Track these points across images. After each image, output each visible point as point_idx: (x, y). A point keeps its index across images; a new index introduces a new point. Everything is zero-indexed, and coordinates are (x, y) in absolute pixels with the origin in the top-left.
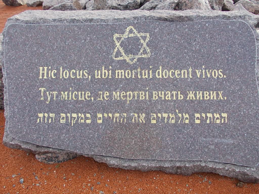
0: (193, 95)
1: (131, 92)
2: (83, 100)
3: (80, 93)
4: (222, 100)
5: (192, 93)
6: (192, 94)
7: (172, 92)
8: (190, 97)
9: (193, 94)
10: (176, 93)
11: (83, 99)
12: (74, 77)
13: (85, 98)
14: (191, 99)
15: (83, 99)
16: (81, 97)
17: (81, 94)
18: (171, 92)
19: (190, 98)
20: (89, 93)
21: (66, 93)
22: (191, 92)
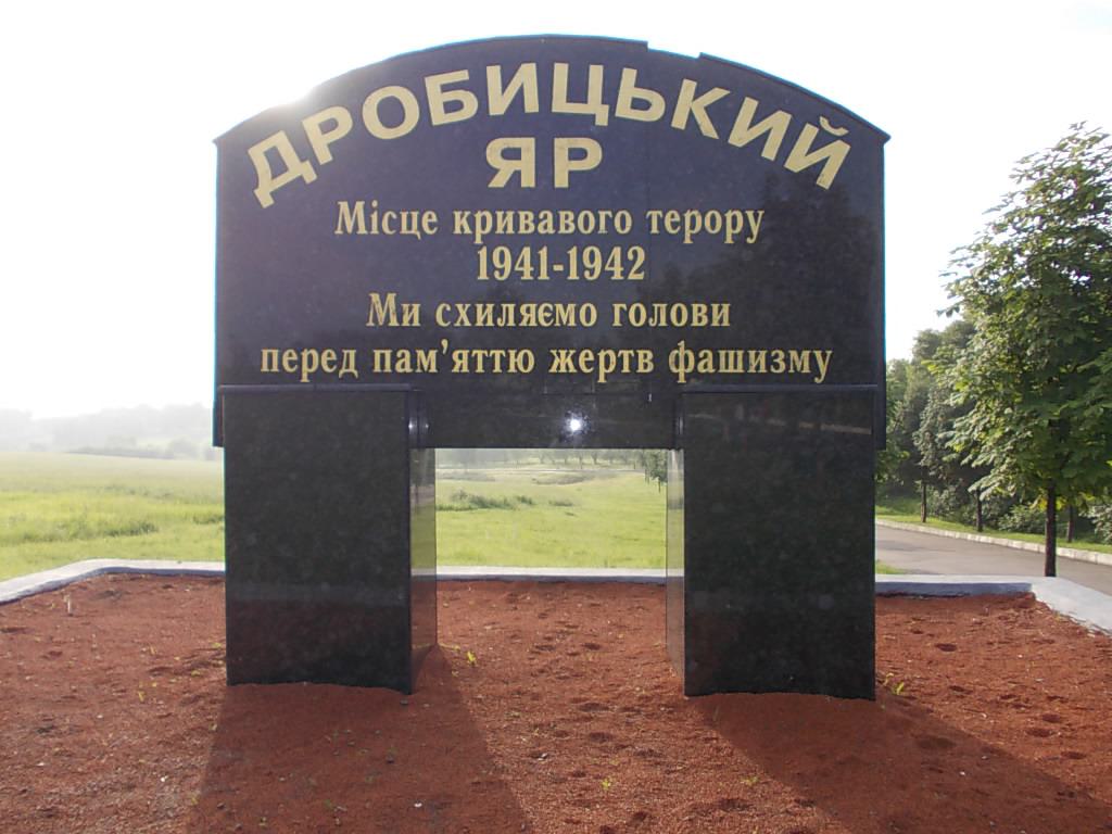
0: (569, 360)
1: (611, 353)
2: (415, 236)
3: (404, 215)
4: (645, 275)
5: (567, 354)
6: (462, 365)
7: (620, 352)
8: (559, 364)
9: (569, 357)
10: (630, 355)
11: (414, 230)
12: (592, 369)
13: (420, 227)
14: (563, 370)
15: (414, 230)
16: (409, 228)
17: (410, 218)
18: (616, 353)
19: (559, 368)
20: (292, 351)
21: (571, 307)
22: (563, 353)
